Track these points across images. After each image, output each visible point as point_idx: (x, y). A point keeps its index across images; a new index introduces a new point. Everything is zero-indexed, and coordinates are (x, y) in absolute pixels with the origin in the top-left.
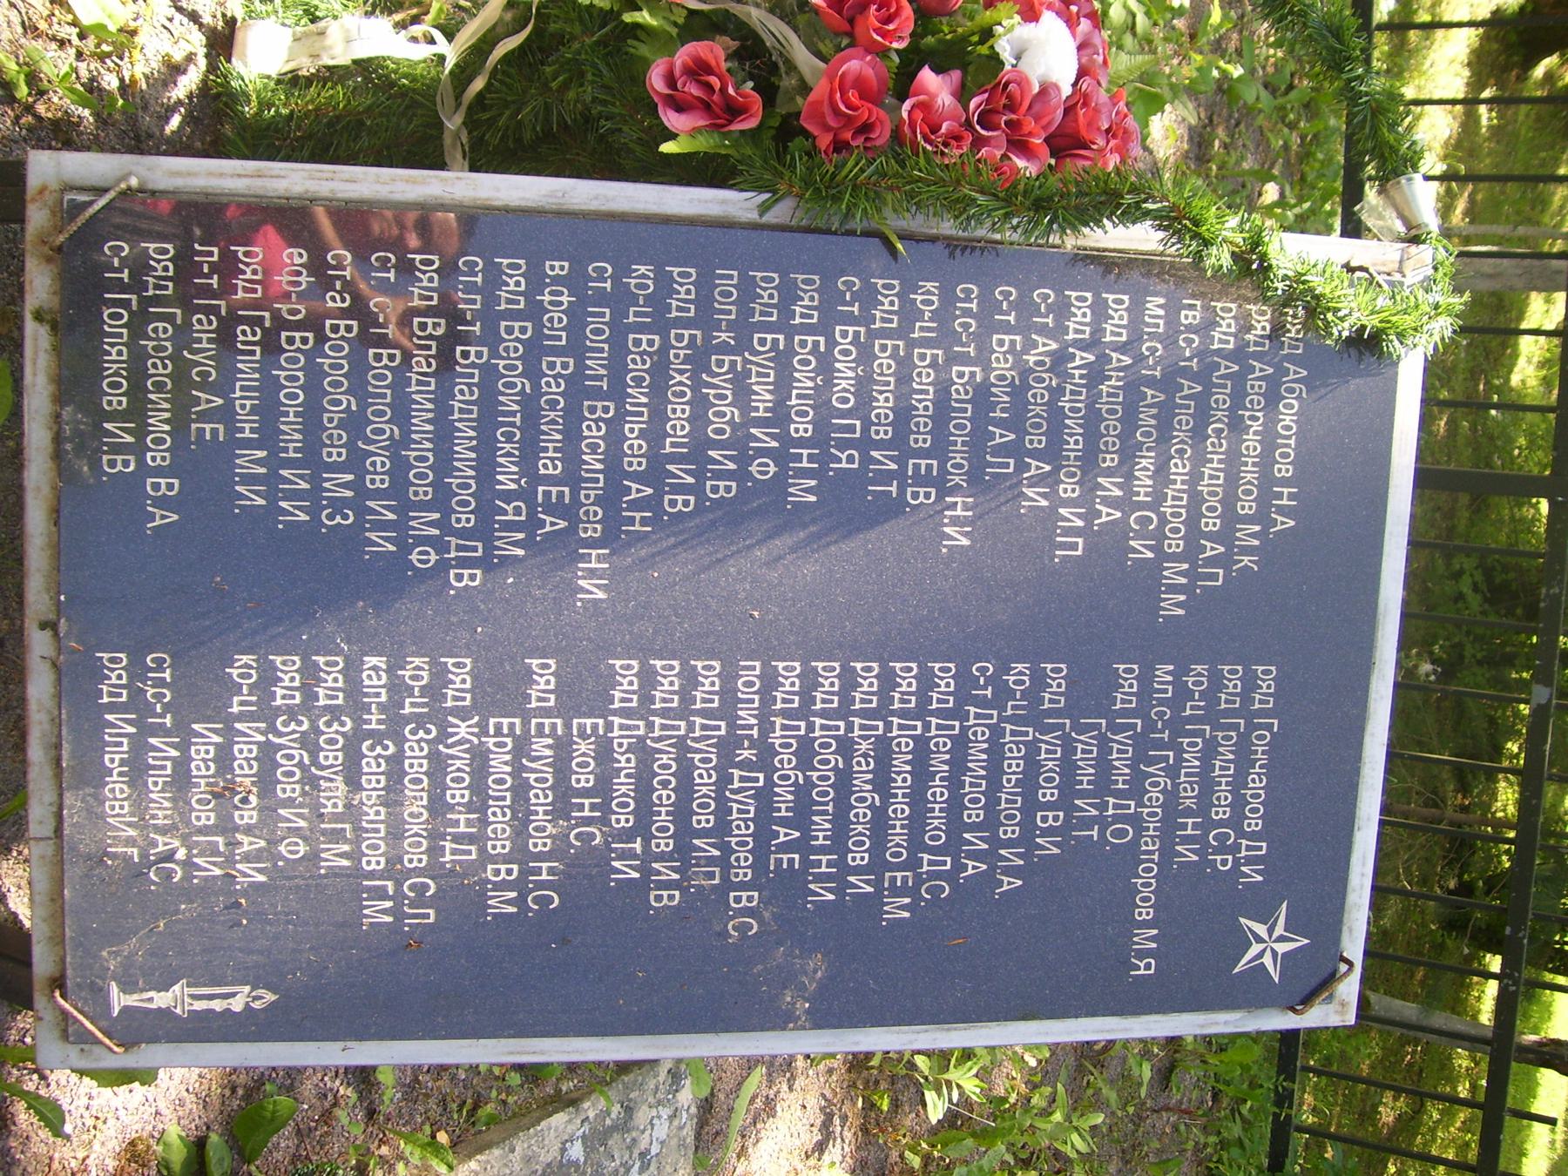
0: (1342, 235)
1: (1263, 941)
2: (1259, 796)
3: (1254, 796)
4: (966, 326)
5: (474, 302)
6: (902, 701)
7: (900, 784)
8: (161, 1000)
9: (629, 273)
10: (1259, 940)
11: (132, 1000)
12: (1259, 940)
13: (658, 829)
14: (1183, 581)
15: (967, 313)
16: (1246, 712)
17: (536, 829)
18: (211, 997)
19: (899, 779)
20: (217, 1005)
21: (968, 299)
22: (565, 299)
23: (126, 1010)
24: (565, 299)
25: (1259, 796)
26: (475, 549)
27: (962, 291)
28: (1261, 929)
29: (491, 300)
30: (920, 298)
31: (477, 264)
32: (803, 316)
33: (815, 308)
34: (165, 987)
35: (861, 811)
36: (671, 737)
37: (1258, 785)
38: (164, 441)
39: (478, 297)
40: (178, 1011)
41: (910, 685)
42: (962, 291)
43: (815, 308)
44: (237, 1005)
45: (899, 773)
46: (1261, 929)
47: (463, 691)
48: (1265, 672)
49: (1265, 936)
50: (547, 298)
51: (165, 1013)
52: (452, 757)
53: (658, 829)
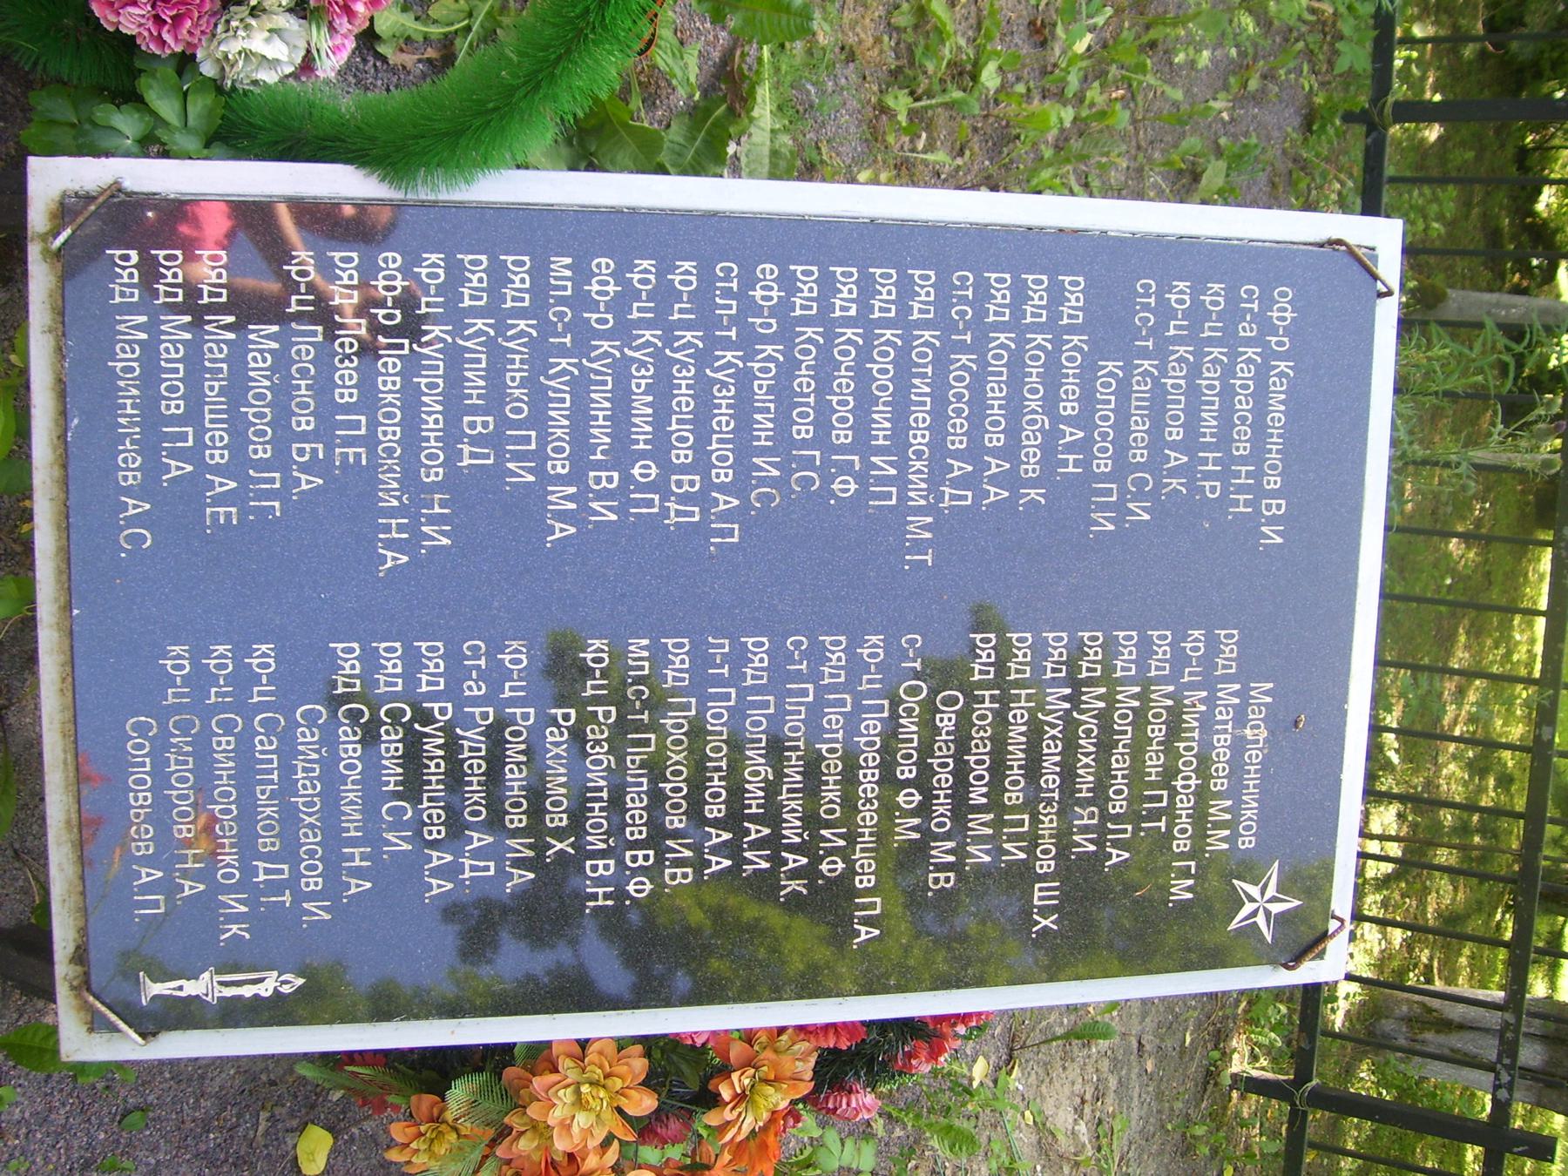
2: (984, 762)
3: (978, 762)
4: (962, 313)
5: (730, 307)
6: (1054, 670)
7: (433, 770)
8: (191, 988)
9: (673, 269)
15: (963, 300)
19: (432, 764)
20: (247, 991)
21: (727, 279)
22: (596, 287)
24: (596, 287)
25: (984, 762)
27: (722, 269)
29: (981, 313)
30: (678, 278)
31: (732, 270)
32: (881, 310)
33: (892, 302)
35: (943, 776)
37: (982, 750)
39: (734, 303)
40: (209, 999)
41: (1096, 653)
42: (722, 269)
43: (892, 302)
44: (266, 989)
45: (431, 758)
47: (394, 675)
50: (774, 294)
52: (427, 735)
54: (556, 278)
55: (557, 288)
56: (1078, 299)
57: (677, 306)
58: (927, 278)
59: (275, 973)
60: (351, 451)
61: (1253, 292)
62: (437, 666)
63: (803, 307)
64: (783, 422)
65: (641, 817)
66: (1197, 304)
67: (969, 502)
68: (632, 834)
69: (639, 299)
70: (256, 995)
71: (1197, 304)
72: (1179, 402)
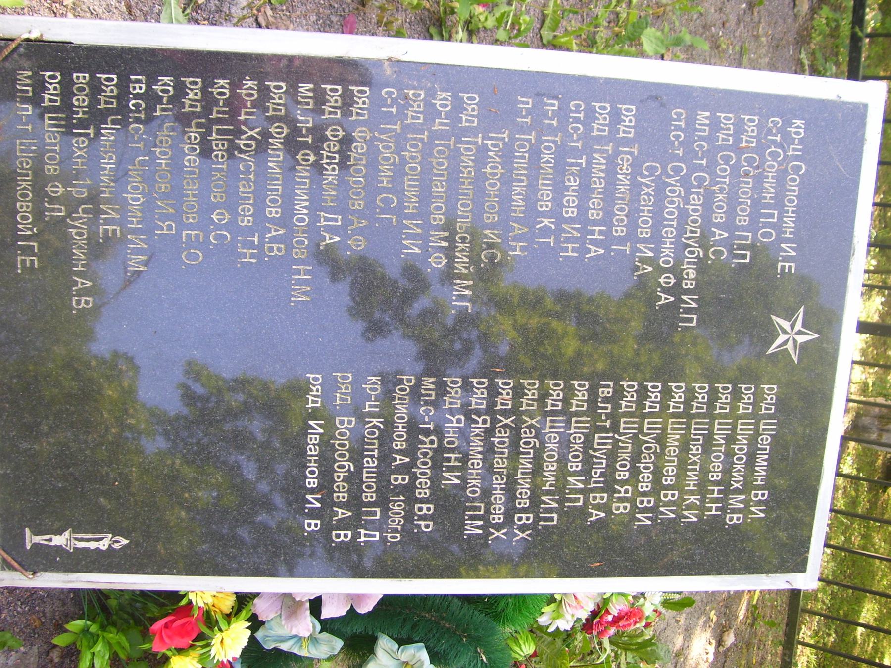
0: (865, 106)
1: (794, 339)
8: (58, 540)
10: (785, 332)
11: (38, 539)
12: (785, 332)
13: (398, 418)
14: (742, 506)
16: (756, 416)
17: (397, 436)
18: (88, 540)
20: (92, 545)
23: (35, 546)
26: (336, 220)
28: (786, 325)
29: (589, 129)
34: (60, 532)
36: (602, 449)
38: (84, 89)
42: (675, 114)
44: (104, 545)
46: (786, 325)
48: (770, 389)
49: (788, 329)
51: (59, 548)
53: (398, 418)
54: (699, 124)
55: (700, 130)
56: (630, 121)
57: (215, 109)
58: (605, 108)
59: (110, 536)
60: (787, 265)
61: (681, 114)
62: (632, 396)
63: (599, 130)
64: (731, 213)
65: (648, 478)
66: (234, 96)
67: (748, 261)
68: (642, 487)
69: (218, 105)
70: (97, 548)
71: (234, 96)
72: (794, 191)
